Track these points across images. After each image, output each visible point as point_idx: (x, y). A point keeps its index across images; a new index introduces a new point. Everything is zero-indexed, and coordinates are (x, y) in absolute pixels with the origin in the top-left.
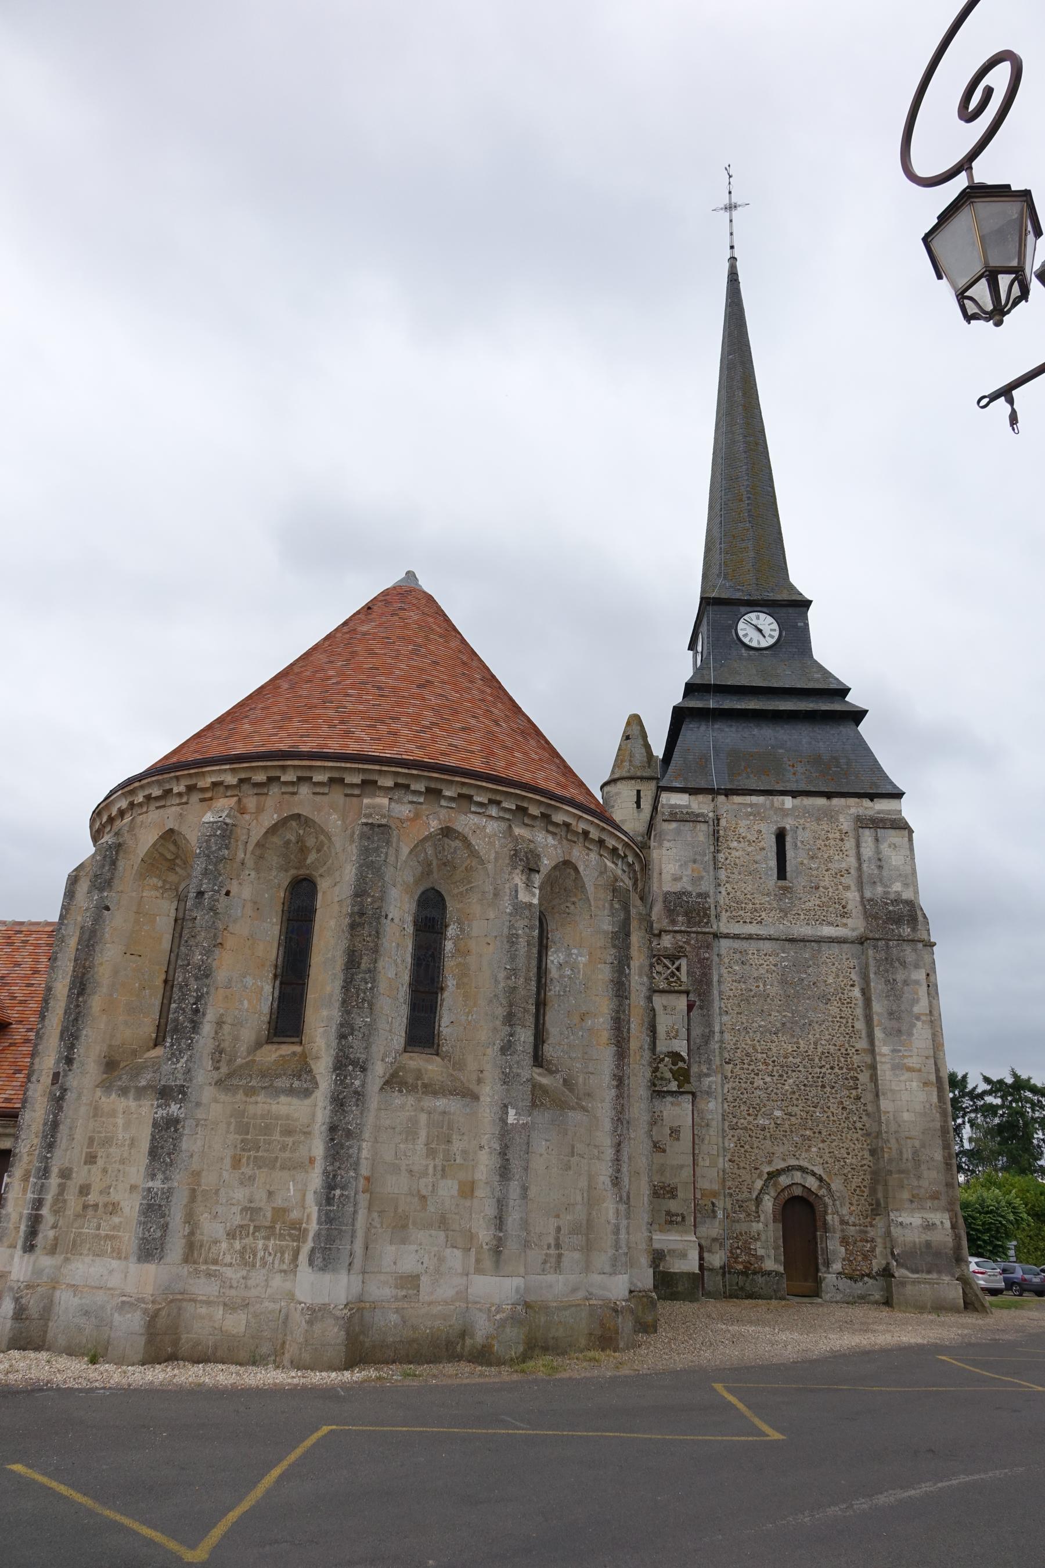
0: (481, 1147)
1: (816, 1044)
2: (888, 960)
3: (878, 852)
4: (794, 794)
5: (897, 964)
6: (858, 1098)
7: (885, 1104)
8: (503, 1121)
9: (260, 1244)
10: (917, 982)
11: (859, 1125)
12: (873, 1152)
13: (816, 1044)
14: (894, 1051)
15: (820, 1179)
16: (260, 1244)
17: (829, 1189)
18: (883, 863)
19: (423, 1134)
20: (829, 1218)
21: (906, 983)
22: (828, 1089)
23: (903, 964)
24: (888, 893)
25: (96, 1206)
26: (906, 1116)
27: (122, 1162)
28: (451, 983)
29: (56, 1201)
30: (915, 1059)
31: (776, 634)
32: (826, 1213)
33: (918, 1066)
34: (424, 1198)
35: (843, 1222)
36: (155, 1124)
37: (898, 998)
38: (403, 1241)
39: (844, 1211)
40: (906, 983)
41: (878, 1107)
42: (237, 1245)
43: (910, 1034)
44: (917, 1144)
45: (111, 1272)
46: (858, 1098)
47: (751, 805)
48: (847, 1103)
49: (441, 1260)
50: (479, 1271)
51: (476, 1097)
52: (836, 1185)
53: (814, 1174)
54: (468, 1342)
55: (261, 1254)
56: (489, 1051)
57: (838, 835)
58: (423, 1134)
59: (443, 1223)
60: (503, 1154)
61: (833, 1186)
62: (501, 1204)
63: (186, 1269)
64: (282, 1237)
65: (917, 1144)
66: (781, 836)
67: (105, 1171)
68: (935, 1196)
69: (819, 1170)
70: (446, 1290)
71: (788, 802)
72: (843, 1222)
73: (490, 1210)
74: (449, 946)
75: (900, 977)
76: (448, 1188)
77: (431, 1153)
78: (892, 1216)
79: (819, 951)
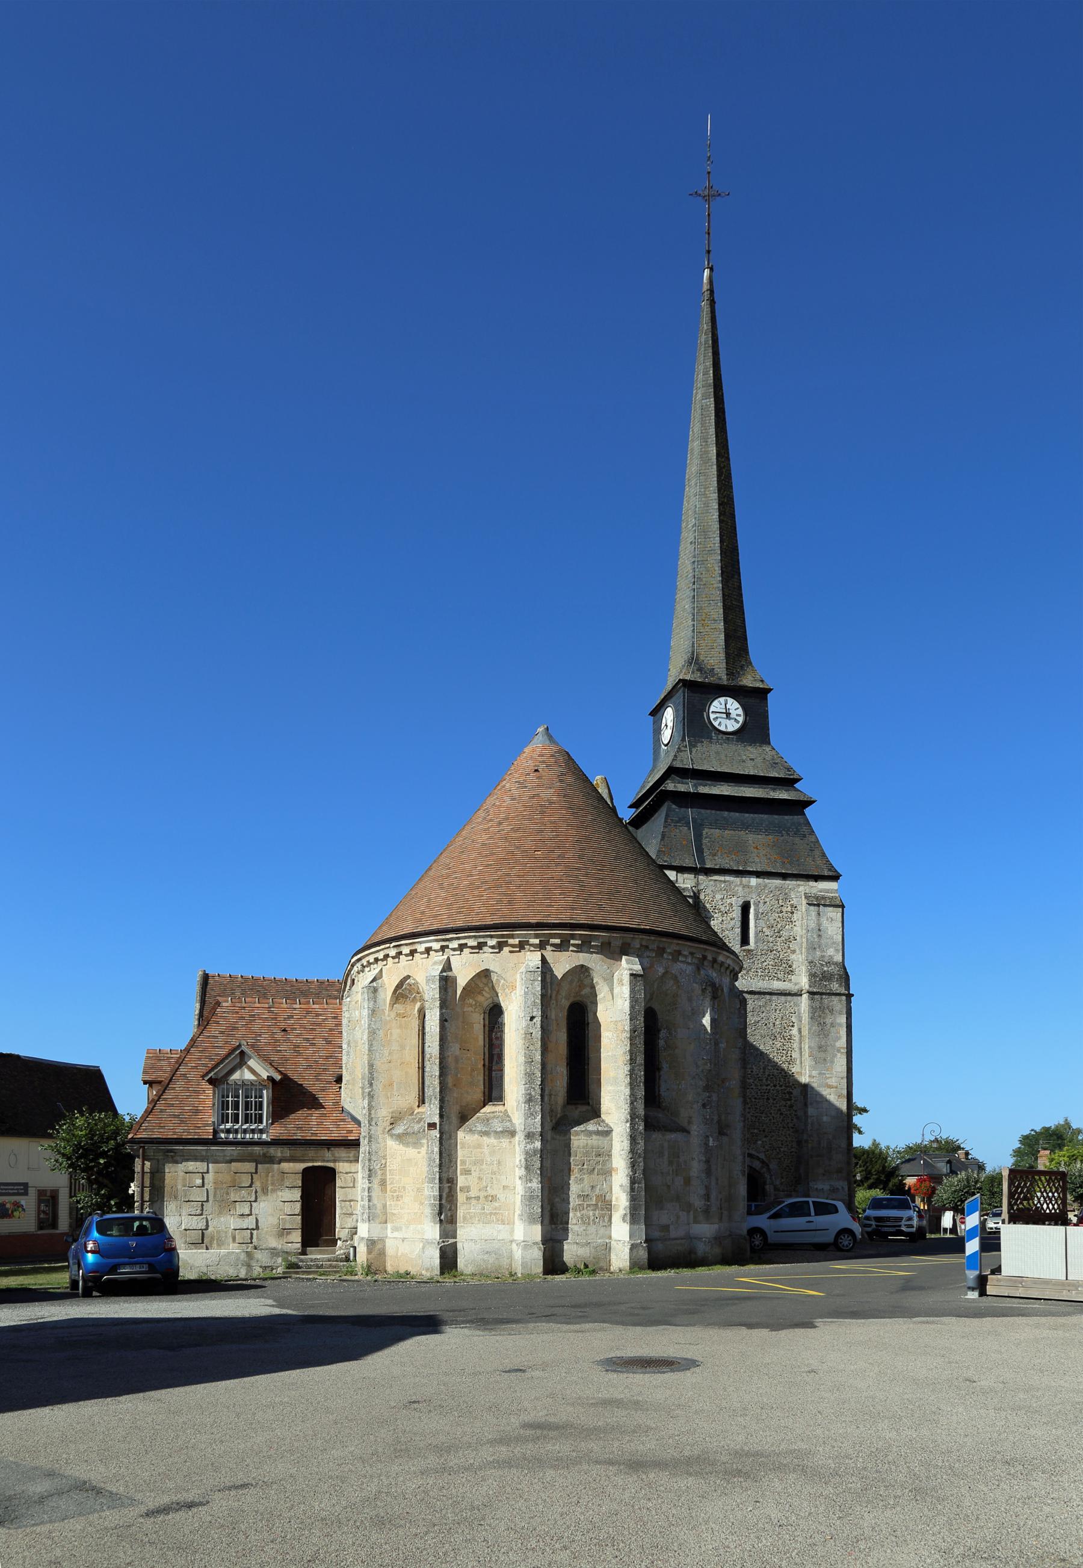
0: (693, 1159)
1: (764, 1069)
2: (822, 1009)
3: (819, 925)
4: (758, 874)
5: (827, 1011)
6: (791, 1106)
7: (811, 1111)
8: (706, 1144)
9: (591, 1213)
10: (840, 1025)
11: (791, 1125)
12: (799, 1143)
13: (764, 1069)
14: (820, 1074)
15: (763, 1162)
16: (591, 1213)
17: (769, 1170)
18: (821, 933)
19: (666, 1153)
20: (767, 1187)
21: (832, 1025)
22: (771, 1101)
23: (831, 1011)
24: (823, 956)
25: (478, 1198)
26: (825, 1119)
27: (494, 1173)
28: (665, 1066)
29: (448, 1196)
30: (834, 1080)
31: (741, 719)
32: (765, 1183)
33: (835, 1084)
34: (669, 1186)
35: (776, 1189)
36: (527, 1153)
37: (826, 1036)
38: (662, 1209)
39: (778, 1182)
40: (832, 1025)
41: (806, 1113)
42: (578, 1214)
43: (832, 1062)
44: (830, 1137)
45: (499, 1231)
46: (791, 1106)
47: (725, 882)
48: (783, 1110)
49: (678, 1217)
50: (696, 1222)
51: (688, 1132)
52: (773, 1166)
53: (758, 1159)
54: (693, 1256)
55: (592, 1218)
56: (695, 1106)
57: (789, 909)
58: (666, 1153)
59: (678, 1198)
60: (707, 1162)
61: (771, 1166)
62: (707, 1188)
63: (576, 1228)
64: (602, 1209)
65: (830, 1137)
66: (745, 908)
67: (480, 1179)
68: (839, 1171)
69: (762, 1156)
70: (681, 1233)
71: (754, 881)
72: (776, 1189)
73: (702, 1192)
74: (661, 1043)
75: (829, 1021)
76: (679, 1181)
77: (670, 1163)
78: (811, 1184)
79: (770, 1000)
